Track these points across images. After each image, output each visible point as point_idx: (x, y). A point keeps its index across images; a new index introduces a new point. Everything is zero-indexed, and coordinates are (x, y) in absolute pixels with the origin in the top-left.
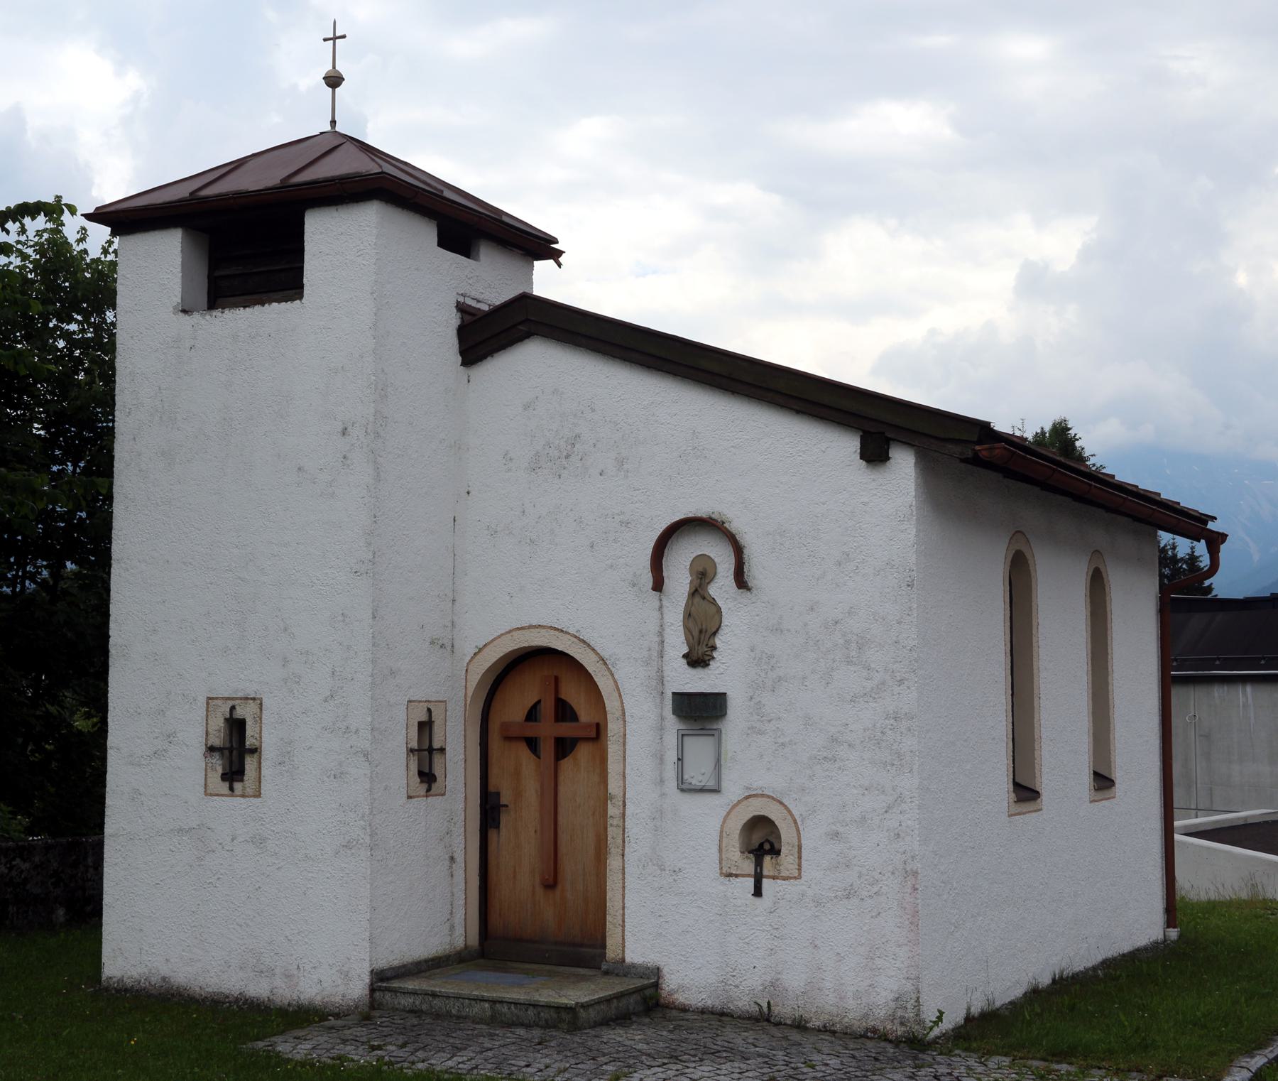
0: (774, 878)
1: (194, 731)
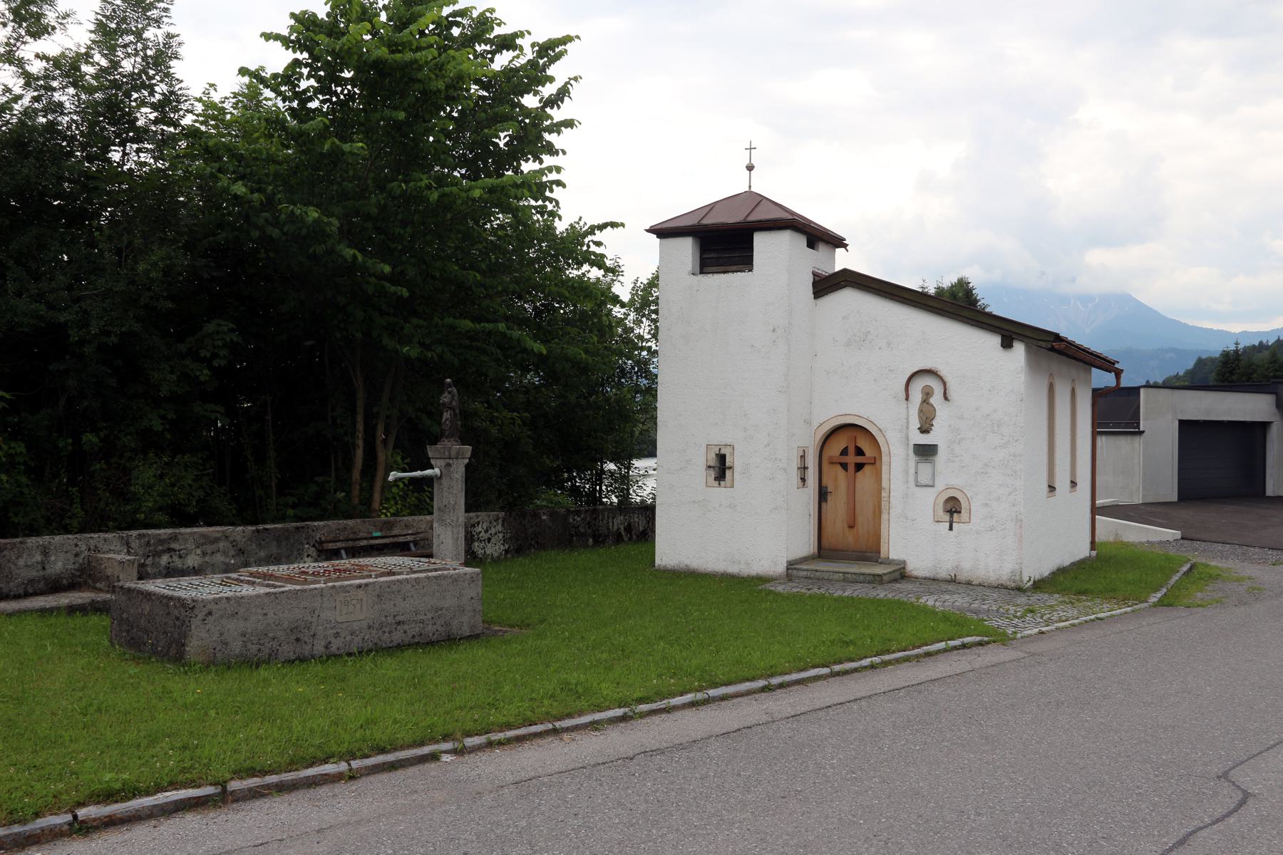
1: (701, 459)
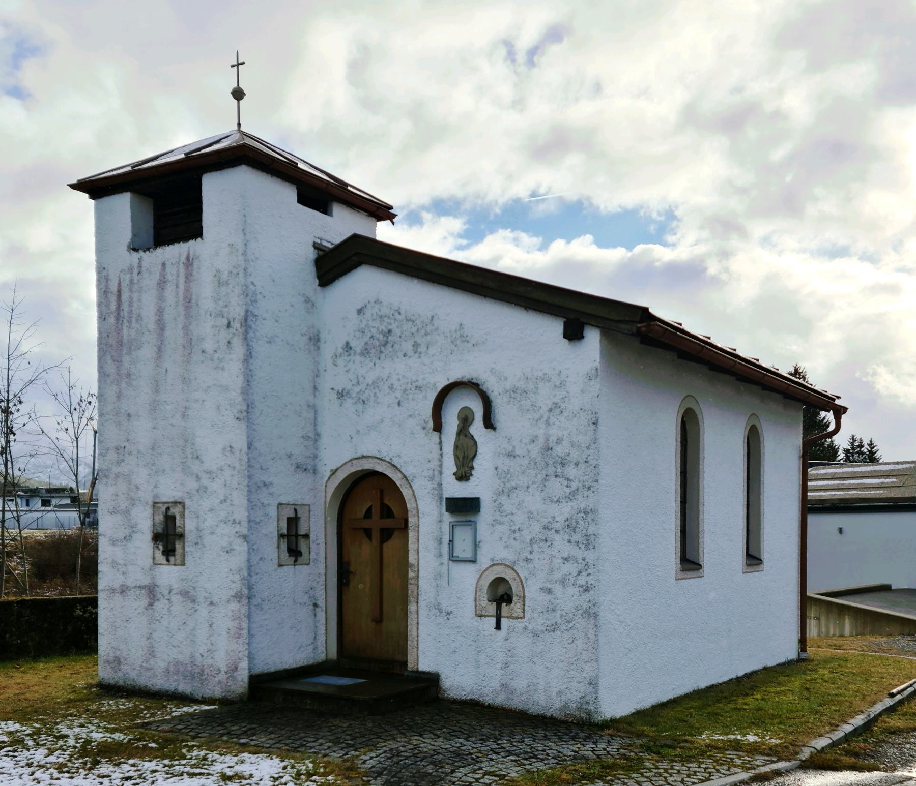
0: (508, 617)
1: (146, 522)
